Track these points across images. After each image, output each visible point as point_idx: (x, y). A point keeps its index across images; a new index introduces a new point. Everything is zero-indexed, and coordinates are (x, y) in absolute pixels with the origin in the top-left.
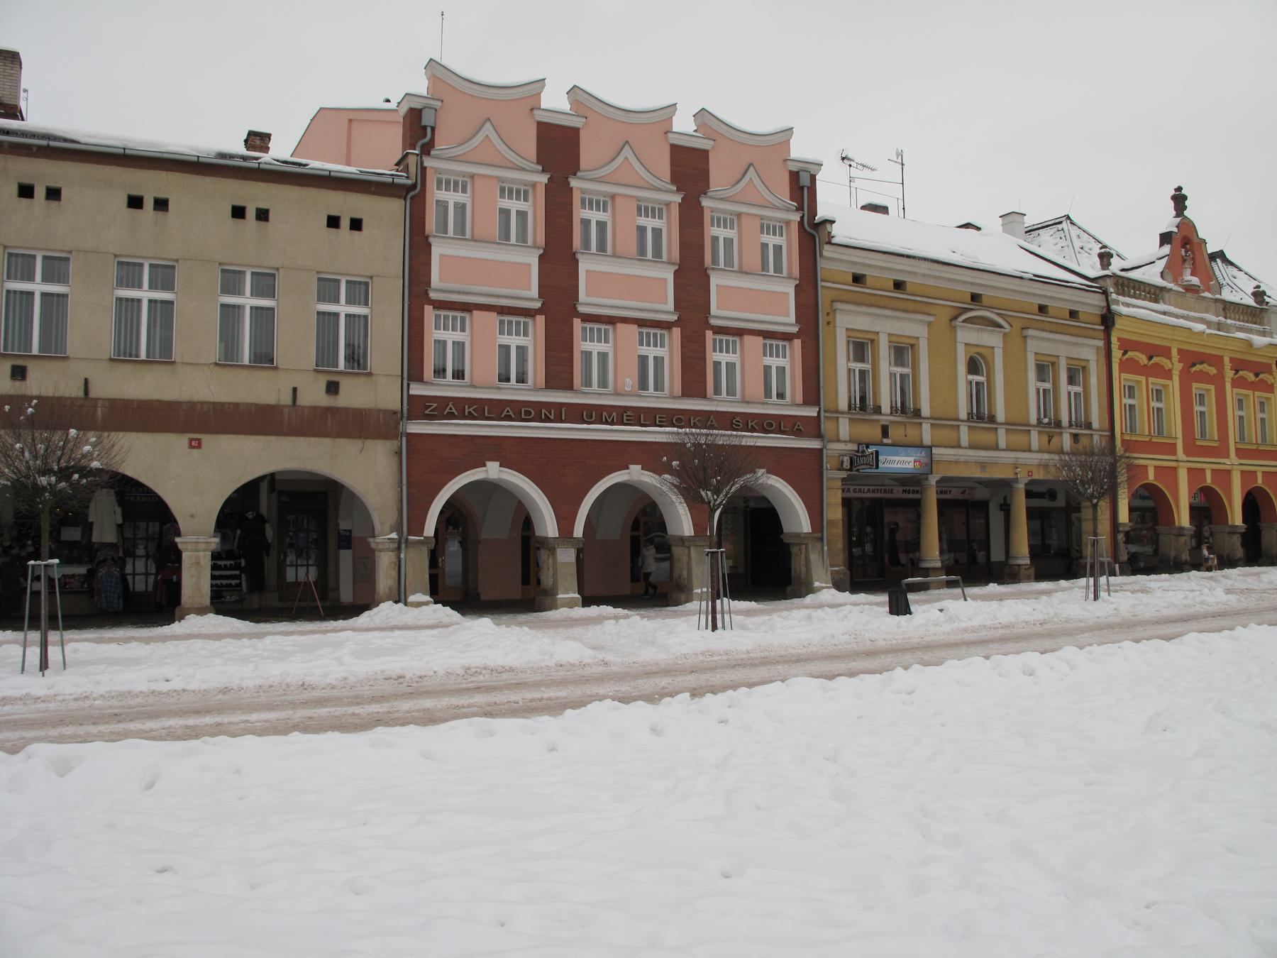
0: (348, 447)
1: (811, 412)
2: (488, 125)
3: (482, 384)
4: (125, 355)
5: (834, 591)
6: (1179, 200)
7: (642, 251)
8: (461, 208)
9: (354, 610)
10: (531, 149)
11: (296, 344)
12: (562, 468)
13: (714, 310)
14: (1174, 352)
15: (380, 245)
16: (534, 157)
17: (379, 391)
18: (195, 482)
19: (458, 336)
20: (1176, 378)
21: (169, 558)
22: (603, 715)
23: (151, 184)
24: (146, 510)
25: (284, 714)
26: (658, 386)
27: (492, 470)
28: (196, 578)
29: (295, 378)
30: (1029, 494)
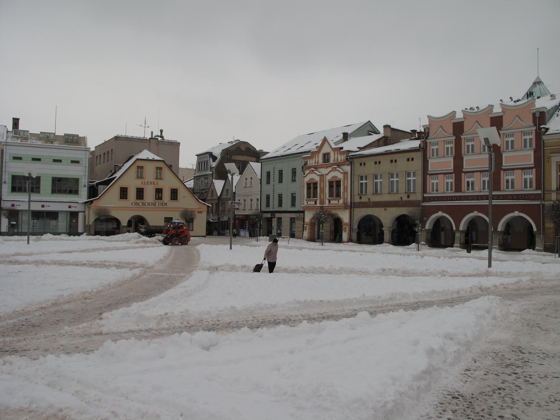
1: (539, 192)
2: (517, 118)
5: (427, 247)
6: (161, 131)
7: (525, 146)
8: (512, 141)
9: (445, 246)
12: (458, 213)
13: (464, 167)
15: (417, 164)
16: (452, 133)
17: (418, 197)
18: (387, 218)
22: (131, 250)
23: (377, 159)
27: (516, 213)
28: (387, 236)
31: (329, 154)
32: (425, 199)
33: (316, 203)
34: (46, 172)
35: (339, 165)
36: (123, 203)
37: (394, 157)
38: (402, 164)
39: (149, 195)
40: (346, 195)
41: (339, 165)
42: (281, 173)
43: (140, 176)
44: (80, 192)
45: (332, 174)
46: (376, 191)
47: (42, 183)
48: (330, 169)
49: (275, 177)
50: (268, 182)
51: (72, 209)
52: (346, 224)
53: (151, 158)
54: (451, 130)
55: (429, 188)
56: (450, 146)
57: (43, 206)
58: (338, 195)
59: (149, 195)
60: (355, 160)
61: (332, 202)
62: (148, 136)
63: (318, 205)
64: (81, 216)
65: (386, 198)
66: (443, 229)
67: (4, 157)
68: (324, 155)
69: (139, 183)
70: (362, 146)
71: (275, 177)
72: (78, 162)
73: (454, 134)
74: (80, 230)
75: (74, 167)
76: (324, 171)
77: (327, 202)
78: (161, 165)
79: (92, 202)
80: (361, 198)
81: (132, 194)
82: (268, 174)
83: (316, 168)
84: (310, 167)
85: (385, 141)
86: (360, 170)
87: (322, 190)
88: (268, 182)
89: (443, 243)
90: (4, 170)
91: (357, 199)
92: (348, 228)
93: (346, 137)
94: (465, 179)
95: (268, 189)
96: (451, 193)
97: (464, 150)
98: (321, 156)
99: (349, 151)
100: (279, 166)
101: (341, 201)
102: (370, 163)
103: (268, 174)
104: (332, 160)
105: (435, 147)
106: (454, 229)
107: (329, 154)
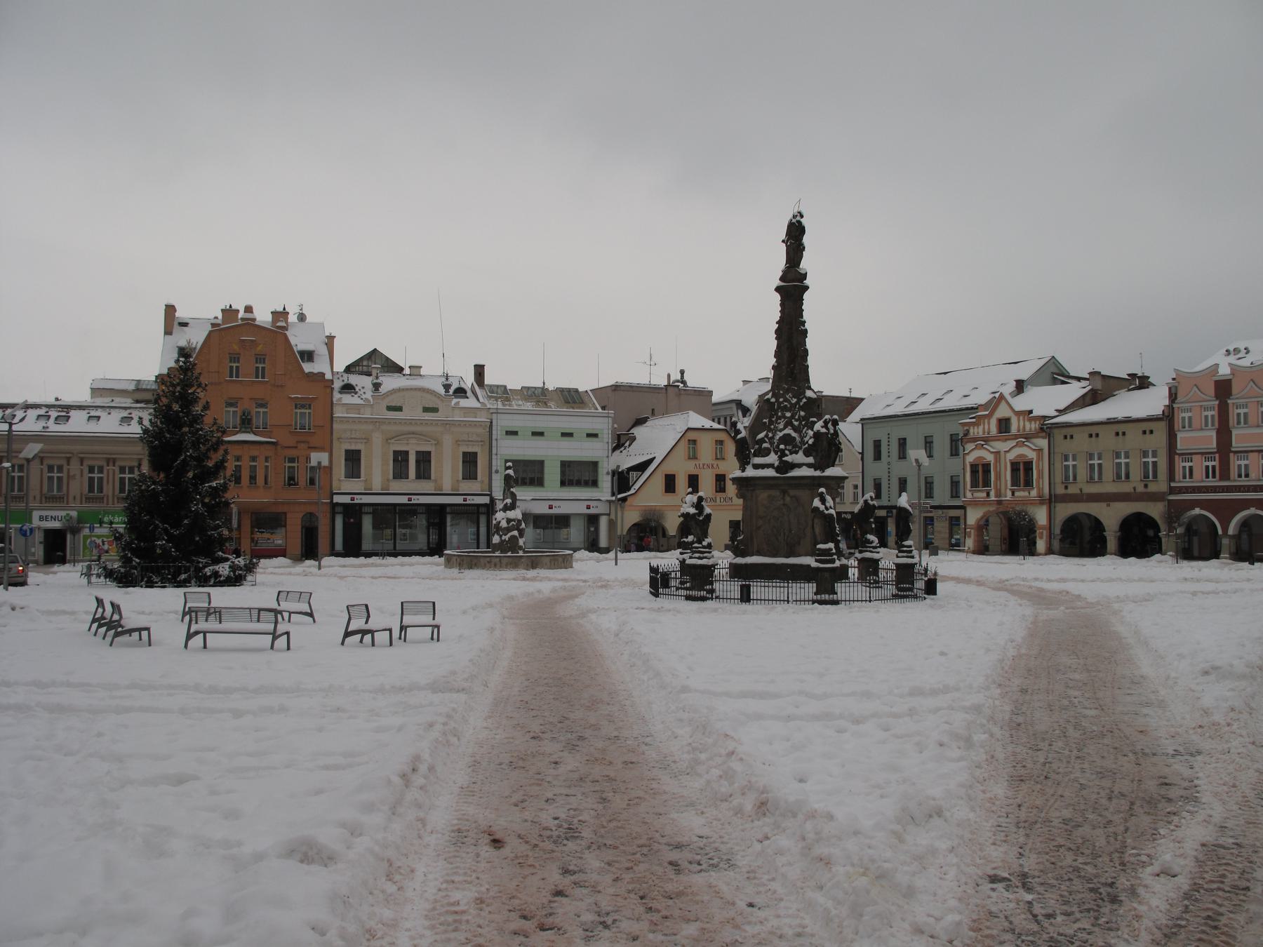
0: (1151, 504)
3: (1199, 479)
4: (1091, 480)
6: (682, 372)
11: (1136, 474)
12: (1226, 510)
13: (1234, 444)
15: (1159, 439)
17: (1161, 486)
18: (1111, 517)
19: (1246, 462)
21: (1103, 541)
23: (1094, 430)
24: (1097, 525)
26: (1214, 476)
27: (1253, 511)
28: (1112, 543)
29: (1135, 483)
32: (1172, 491)
33: (988, 495)
34: (553, 452)
35: (1028, 437)
36: (670, 499)
37: (1121, 428)
38: (1134, 439)
40: (1042, 484)
41: (1028, 437)
42: (903, 443)
43: (693, 456)
44: (600, 483)
45: (1012, 451)
47: (546, 470)
48: (1013, 443)
50: (878, 456)
51: (592, 511)
52: (1042, 527)
53: (707, 426)
54: (1211, 391)
55: (1179, 474)
56: (1209, 413)
57: (551, 507)
60: (1056, 431)
61: (1017, 494)
63: (993, 498)
64: (603, 522)
65: (1109, 488)
67: (494, 432)
69: (690, 467)
70: (1062, 407)
72: (595, 435)
73: (1217, 397)
74: (603, 543)
75: (592, 443)
76: (1001, 446)
77: (1009, 493)
78: (722, 436)
79: (624, 500)
80: (1066, 488)
82: (877, 444)
83: (987, 440)
84: (974, 440)
85: (1092, 398)
86: (1063, 446)
87: (998, 477)
88: (878, 456)
89: (1196, 553)
90: (494, 451)
91: (1060, 490)
92: (1045, 533)
93: (1020, 386)
95: (877, 470)
97: (1232, 420)
98: (994, 422)
99: (1044, 417)
100: (899, 431)
101: (1034, 493)
102: (1081, 439)
103: (877, 444)
104: (1014, 429)
105: (1186, 415)
106: (1220, 532)
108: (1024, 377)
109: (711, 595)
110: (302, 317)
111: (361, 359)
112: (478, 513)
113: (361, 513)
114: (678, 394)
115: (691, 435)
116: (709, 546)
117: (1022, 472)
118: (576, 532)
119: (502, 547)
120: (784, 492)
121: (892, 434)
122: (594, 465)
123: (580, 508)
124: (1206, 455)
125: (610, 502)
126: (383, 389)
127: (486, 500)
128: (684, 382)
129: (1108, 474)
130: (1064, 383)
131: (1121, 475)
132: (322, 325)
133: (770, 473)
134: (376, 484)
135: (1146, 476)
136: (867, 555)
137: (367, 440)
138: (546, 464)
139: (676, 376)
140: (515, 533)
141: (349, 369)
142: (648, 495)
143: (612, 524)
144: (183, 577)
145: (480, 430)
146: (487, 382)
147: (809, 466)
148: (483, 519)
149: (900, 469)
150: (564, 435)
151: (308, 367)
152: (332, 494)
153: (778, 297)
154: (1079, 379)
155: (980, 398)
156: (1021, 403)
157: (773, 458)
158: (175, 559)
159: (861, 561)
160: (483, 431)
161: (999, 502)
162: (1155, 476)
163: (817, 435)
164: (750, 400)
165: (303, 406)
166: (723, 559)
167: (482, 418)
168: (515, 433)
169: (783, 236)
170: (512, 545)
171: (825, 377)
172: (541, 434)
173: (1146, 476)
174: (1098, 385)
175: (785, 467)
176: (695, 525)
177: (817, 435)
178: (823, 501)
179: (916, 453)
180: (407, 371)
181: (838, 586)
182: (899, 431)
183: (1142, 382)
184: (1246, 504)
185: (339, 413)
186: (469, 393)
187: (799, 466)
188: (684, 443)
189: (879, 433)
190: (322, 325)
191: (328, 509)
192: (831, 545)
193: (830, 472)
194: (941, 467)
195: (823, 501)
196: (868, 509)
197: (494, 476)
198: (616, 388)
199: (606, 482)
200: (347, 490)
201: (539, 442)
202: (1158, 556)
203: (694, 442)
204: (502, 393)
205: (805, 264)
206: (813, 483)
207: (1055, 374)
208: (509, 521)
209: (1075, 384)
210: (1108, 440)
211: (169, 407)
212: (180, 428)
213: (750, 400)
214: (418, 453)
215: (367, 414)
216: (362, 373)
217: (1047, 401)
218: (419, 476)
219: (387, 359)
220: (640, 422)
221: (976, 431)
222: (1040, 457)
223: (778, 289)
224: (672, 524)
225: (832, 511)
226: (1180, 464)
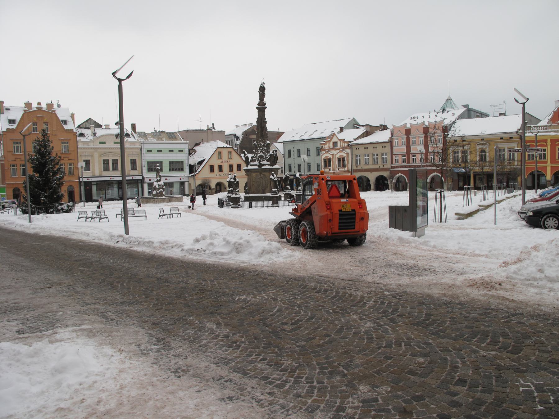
3: (400, 163)
6: (213, 124)
10: (404, 133)
11: (380, 161)
14: (549, 141)
15: (388, 149)
17: (388, 166)
18: (372, 177)
20: (549, 147)
23: (366, 146)
24: (368, 181)
25: (438, 200)
27: (435, 173)
28: (372, 186)
30: (497, 174)
31: (336, 143)
32: (392, 167)
34: (166, 158)
35: (343, 149)
36: (212, 175)
37: (375, 145)
38: (379, 150)
39: (226, 169)
41: (343, 149)
42: (299, 151)
43: (220, 158)
45: (338, 154)
46: (366, 163)
48: (338, 151)
49: (294, 153)
50: (290, 156)
51: (182, 180)
57: (150, 180)
58: (344, 166)
59: (226, 169)
60: (353, 147)
62: (206, 128)
64: (186, 185)
66: (401, 182)
68: (334, 143)
69: (219, 162)
71: (294, 153)
72: (182, 151)
73: (406, 135)
75: (181, 154)
76: (334, 152)
78: (231, 150)
81: (216, 169)
82: (289, 152)
83: (329, 150)
84: (325, 150)
85: (366, 134)
86: (356, 152)
88: (290, 156)
89: (401, 189)
91: (355, 168)
93: (341, 129)
94: (412, 157)
95: (289, 161)
96: (405, 164)
98: (332, 143)
100: (297, 146)
101: (346, 169)
102: (362, 150)
103: (289, 152)
104: (339, 146)
105: (397, 141)
107: (336, 143)
108: (343, 126)
109: (239, 206)
110: (59, 106)
111: (85, 122)
112: (138, 183)
113: (91, 185)
114: (211, 134)
115: (219, 150)
116: (238, 191)
117: (342, 161)
118: (176, 189)
119: (157, 195)
120: (261, 173)
121: (295, 147)
122: (182, 162)
123: (178, 179)
124: (402, 155)
125: (189, 177)
126: (97, 135)
127: (141, 178)
128: (214, 128)
129: (371, 161)
130: (357, 128)
131: (375, 161)
132: (67, 109)
133: (256, 167)
134: (97, 173)
135: (384, 162)
136: (287, 192)
137: (92, 156)
138: (163, 163)
139: (211, 126)
140: (162, 190)
141: (79, 127)
142: (203, 174)
143: (190, 185)
144: (51, 210)
145: (137, 150)
146: (137, 130)
147: (268, 165)
148: (140, 185)
149: (299, 161)
150: (170, 151)
151: (66, 127)
152: (79, 178)
153: (257, 110)
154: (363, 126)
155: (327, 134)
156: (341, 136)
157: (257, 163)
158: (48, 204)
159: (285, 194)
160: (139, 151)
161: (334, 173)
162: (386, 162)
163: (271, 155)
164: (239, 134)
165: (65, 143)
166: (242, 195)
167: (138, 146)
168: (151, 151)
169: (258, 90)
170: (161, 194)
171: (271, 127)
172: (161, 151)
173: (384, 162)
174: (369, 129)
175: (261, 165)
176: (234, 185)
177: (271, 155)
178: (273, 176)
179: (304, 156)
180: (104, 127)
181: (279, 202)
182: (297, 146)
183: (385, 128)
184: (434, 171)
185: (80, 145)
186: (131, 136)
187: (265, 165)
188: (216, 153)
189: (288, 147)
190: (67, 109)
191: (78, 183)
192: (276, 189)
193: (275, 167)
194: (314, 160)
195: (273, 176)
196: (287, 177)
197: (144, 168)
198: (187, 131)
199: (187, 169)
200: (86, 176)
201: (160, 154)
202: (387, 190)
203: (220, 152)
204: (143, 135)
205: (265, 100)
206: (270, 170)
207: (355, 125)
208: (159, 185)
209: (362, 128)
210: (371, 149)
211: (40, 149)
212: (45, 157)
213: (239, 134)
214: (113, 160)
215: (91, 145)
216: (85, 128)
217: (350, 135)
218: (113, 170)
219: (95, 122)
220: (198, 144)
221: (325, 147)
222: (348, 156)
223: (257, 108)
224: (213, 186)
225: (276, 179)
226: (394, 158)
